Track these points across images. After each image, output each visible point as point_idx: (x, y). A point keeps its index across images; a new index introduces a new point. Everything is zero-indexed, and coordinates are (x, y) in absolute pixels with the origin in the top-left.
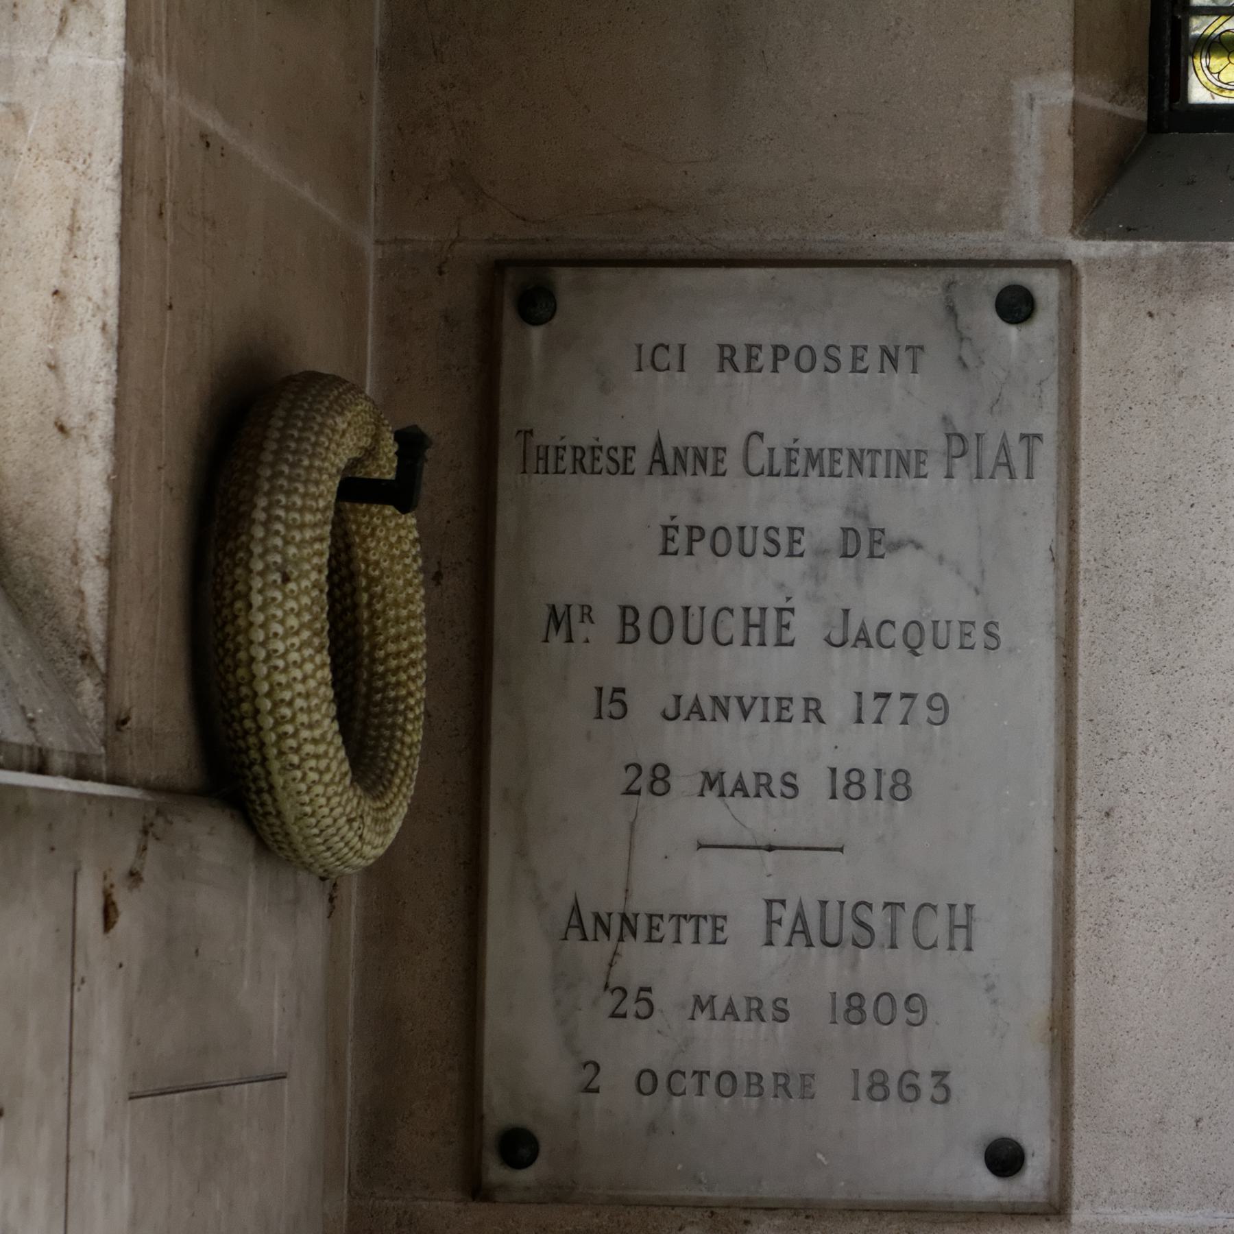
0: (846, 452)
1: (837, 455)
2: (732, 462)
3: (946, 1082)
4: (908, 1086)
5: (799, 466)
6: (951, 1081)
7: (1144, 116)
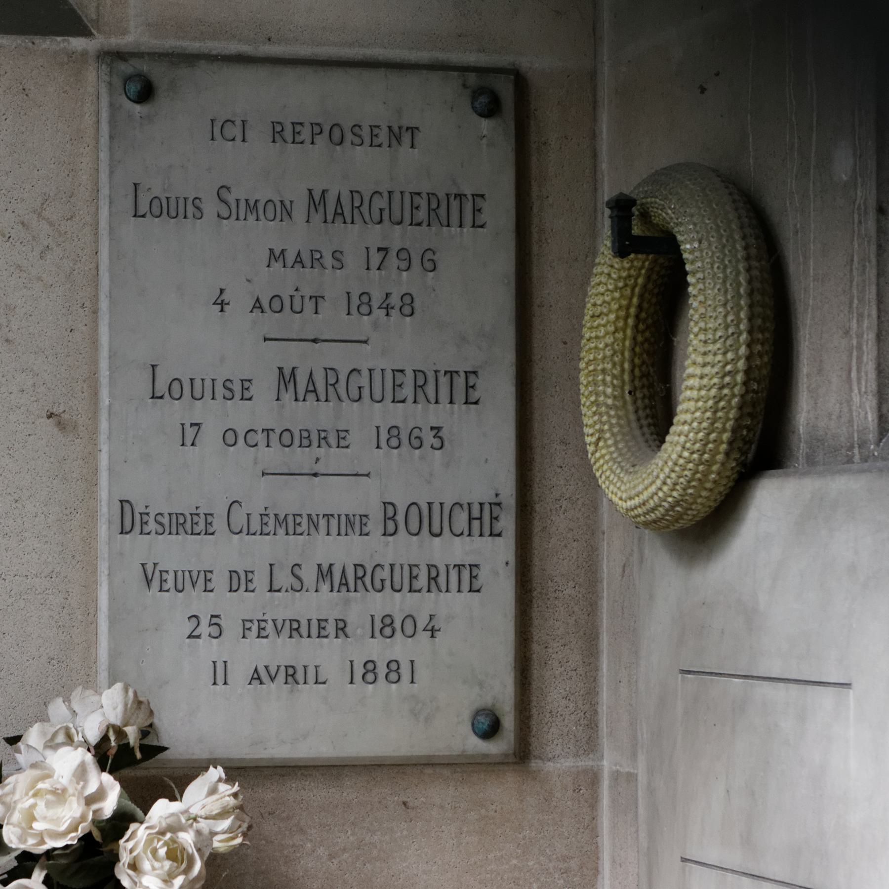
0: (305, 518)
1: (298, 520)
2: (219, 524)
3: (439, 434)
4: (416, 438)
5: (270, 528)
6: (443, 433)
7: (474, 74)
